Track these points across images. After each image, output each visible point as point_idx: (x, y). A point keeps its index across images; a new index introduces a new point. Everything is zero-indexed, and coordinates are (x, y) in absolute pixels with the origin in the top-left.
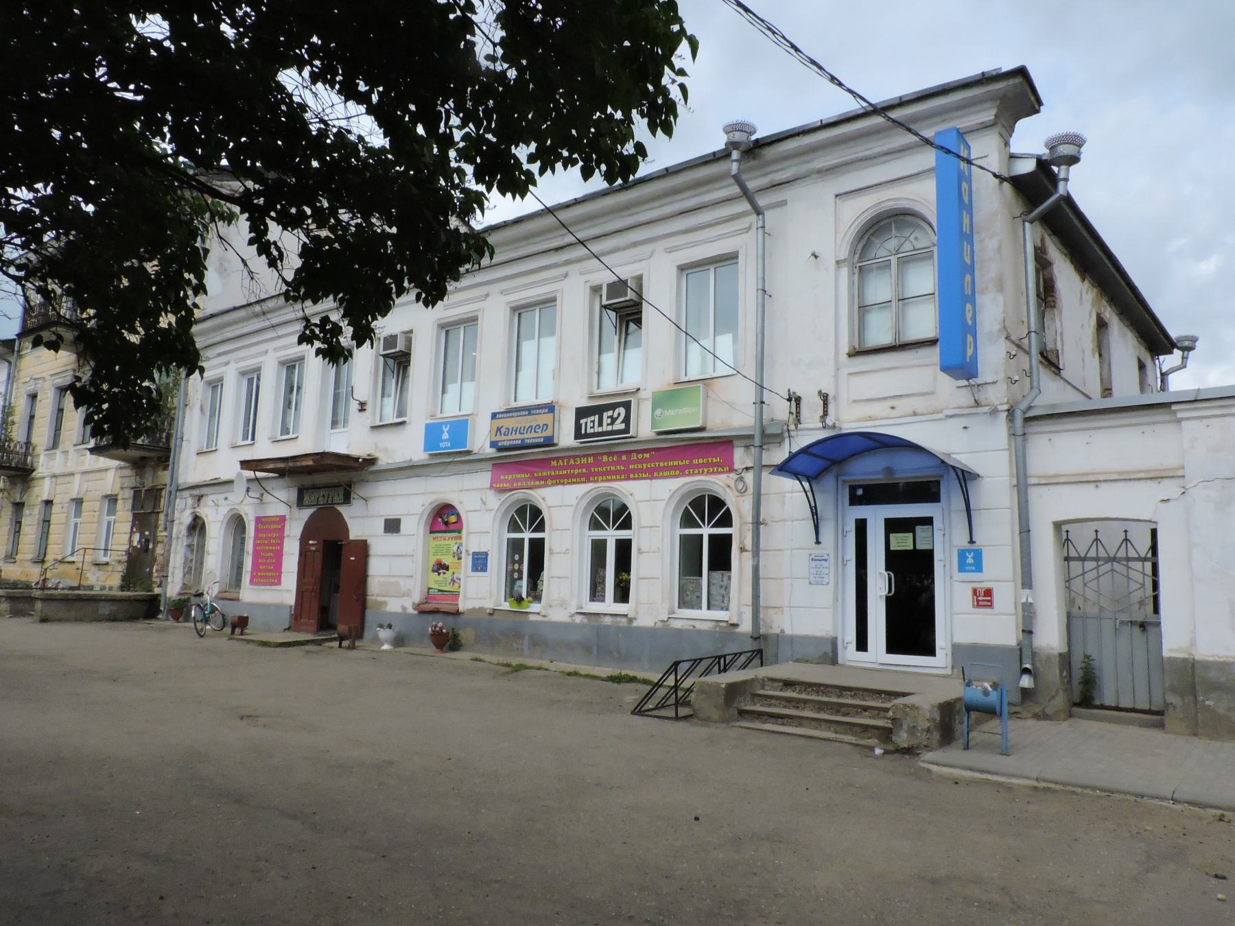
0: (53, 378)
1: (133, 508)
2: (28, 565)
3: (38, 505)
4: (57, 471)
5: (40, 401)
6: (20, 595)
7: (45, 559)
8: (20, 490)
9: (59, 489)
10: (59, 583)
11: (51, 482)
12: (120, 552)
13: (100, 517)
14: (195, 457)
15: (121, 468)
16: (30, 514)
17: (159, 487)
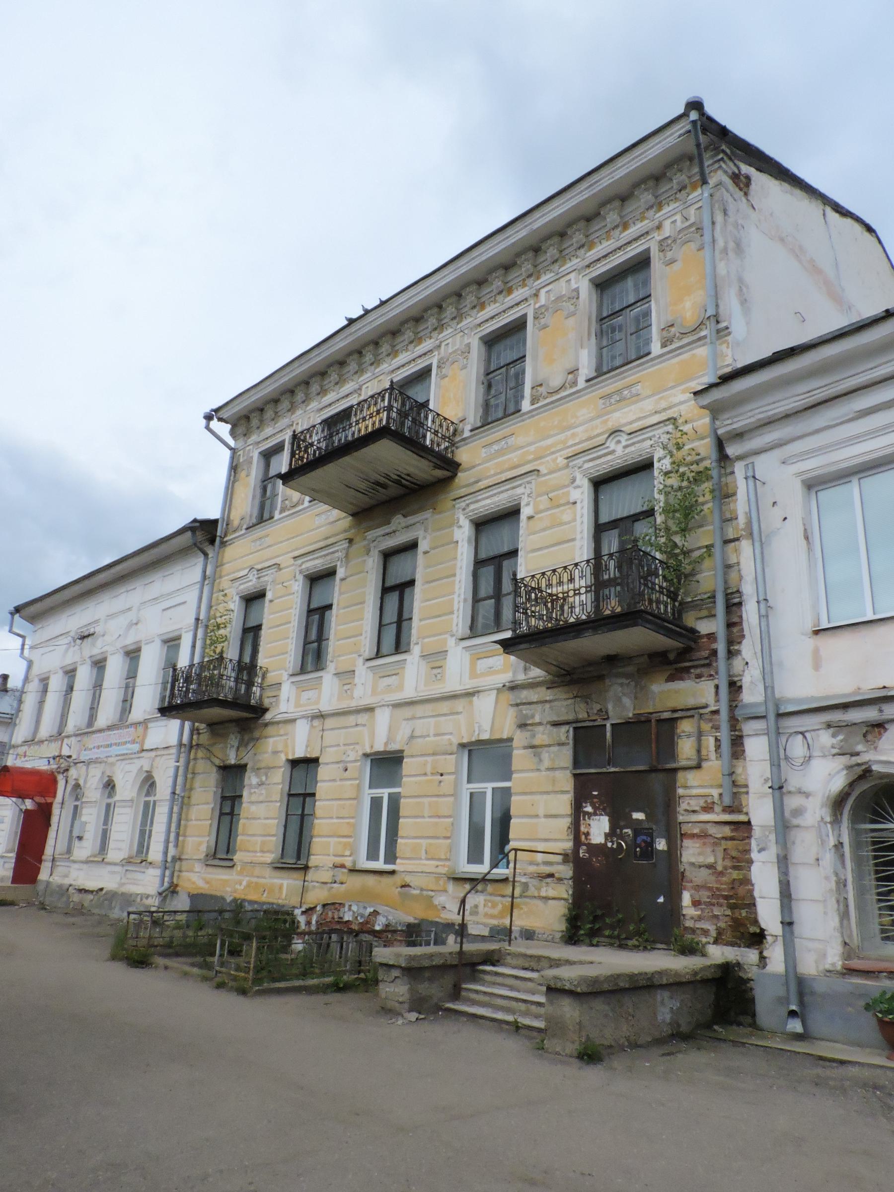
0: (299, 562)
1: (576, 763)
2: (268, 872)
3: (280, 767)
4: (325, 706)
5: (271, 601)
6: (426, 963)
7: (310, 865)
8: (236, 744)
9: (330, 737)
10: (375, 913)
11: (312, 726)
12: (540, 857)
13: (456, 784)
14: (811, 643)
15: (513, 687)
16: (261, 784)
17: (666, 715)
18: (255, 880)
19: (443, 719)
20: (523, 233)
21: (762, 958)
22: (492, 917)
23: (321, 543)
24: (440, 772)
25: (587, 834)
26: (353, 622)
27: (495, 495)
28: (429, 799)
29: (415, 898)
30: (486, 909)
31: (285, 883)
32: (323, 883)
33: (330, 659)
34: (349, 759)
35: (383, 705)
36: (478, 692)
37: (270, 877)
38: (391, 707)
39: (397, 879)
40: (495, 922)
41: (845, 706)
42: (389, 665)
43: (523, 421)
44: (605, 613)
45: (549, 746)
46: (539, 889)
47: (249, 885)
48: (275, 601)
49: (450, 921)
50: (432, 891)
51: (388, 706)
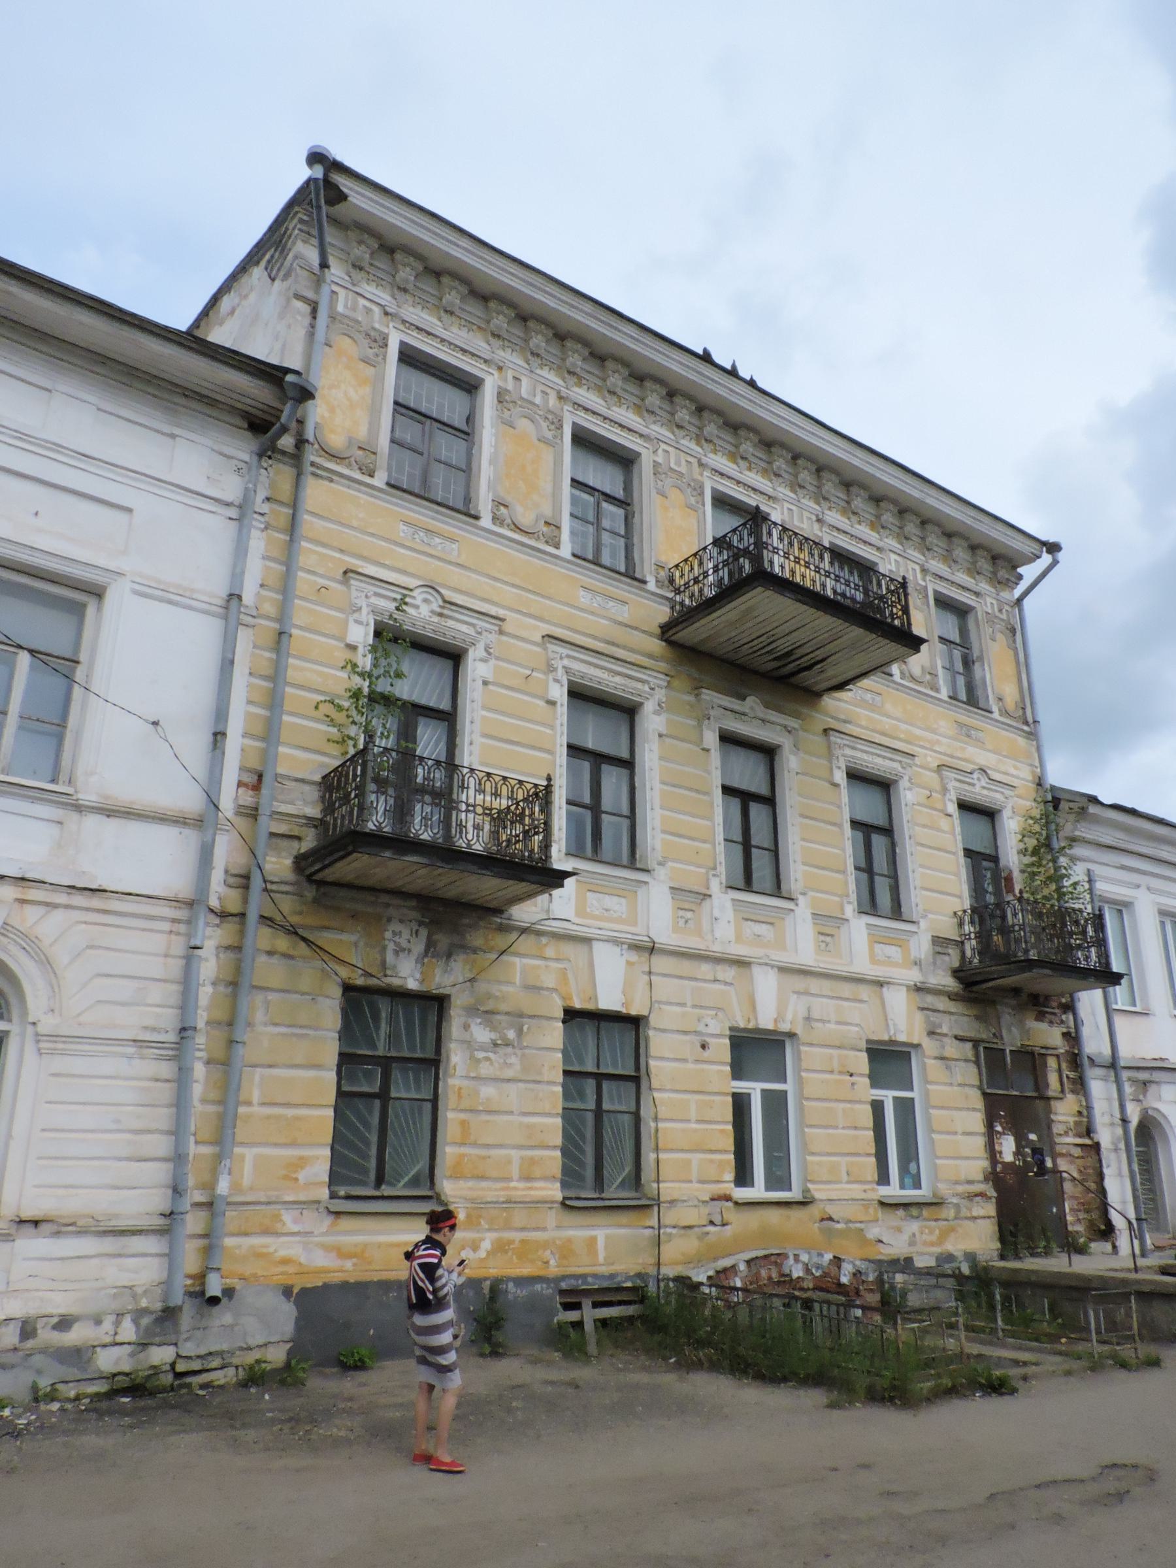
2: (552, 1218)
10: (837, 1261)
15: (919, 989)
18: (517, 1236)
19: (846, 1004)
20: (916, 494)
21: (1114, 1247)
22: (932, 1244)
23: (639, 657)
24: (851, 1071)
25: (1001, 1153)
26: (685, 814)
27: (873, 754)
28: (842, 1105)
29: (841, 1233)
30: (924, 1237)
31: (601, 1234)
32: (685, 1227)
33: (658, 855)
34: (710, 1030)
35: (766, 964)
36: (888, 983)
37: (558, 1227)
38: (776, 970)
39: (815, 1211)
40: (937, 1250)
41: (1138, 1068)
42: (761, 907)
43: (888, 686)
44: (421, 837)
45: (957, 1060)
46: (970, 1210)
47: (500, 1248)
48: (491, 687)
49: (896, 1257)
50: (861, 1222)
51: (772, 966)
